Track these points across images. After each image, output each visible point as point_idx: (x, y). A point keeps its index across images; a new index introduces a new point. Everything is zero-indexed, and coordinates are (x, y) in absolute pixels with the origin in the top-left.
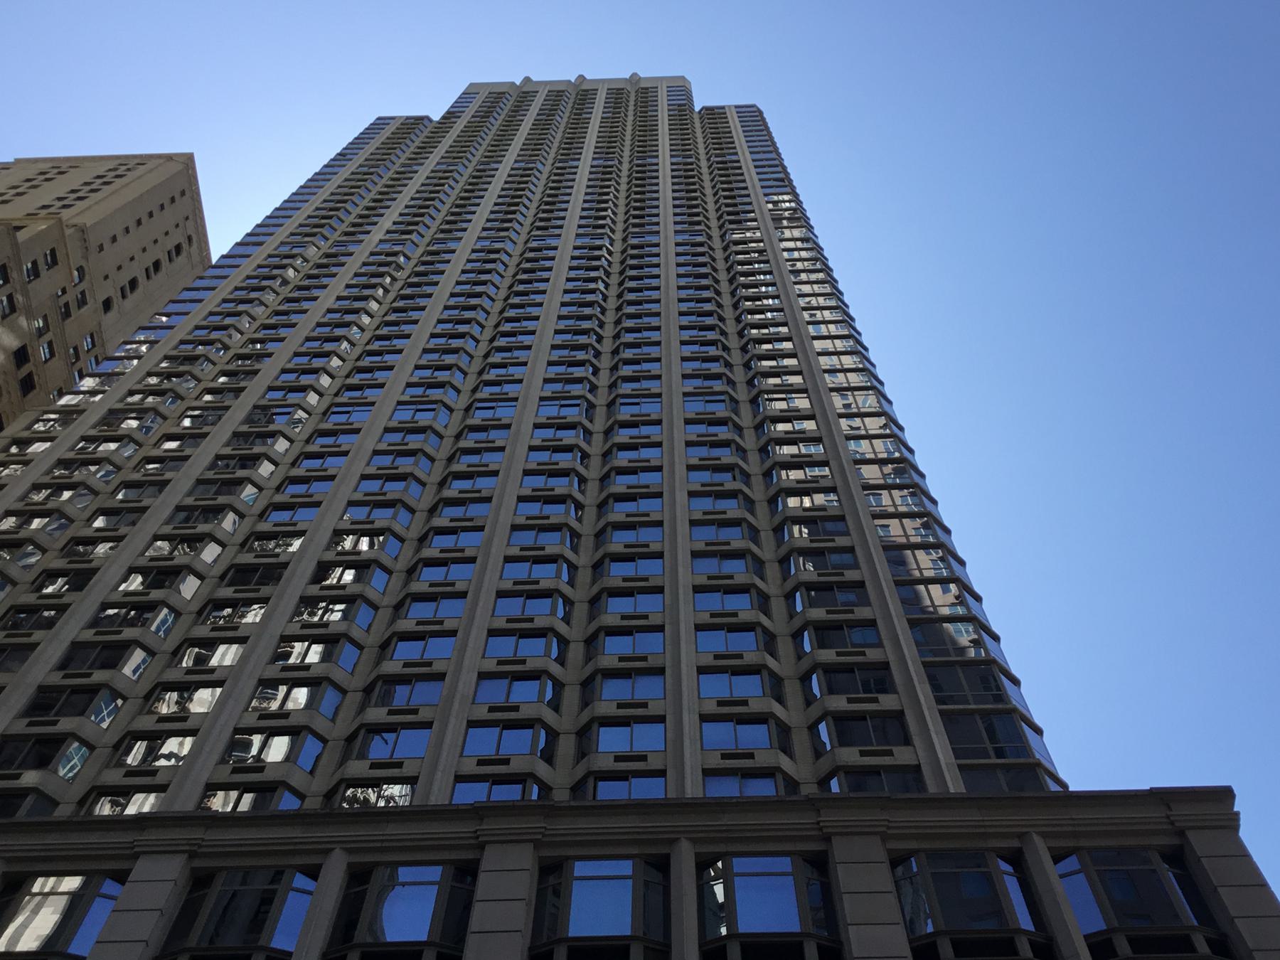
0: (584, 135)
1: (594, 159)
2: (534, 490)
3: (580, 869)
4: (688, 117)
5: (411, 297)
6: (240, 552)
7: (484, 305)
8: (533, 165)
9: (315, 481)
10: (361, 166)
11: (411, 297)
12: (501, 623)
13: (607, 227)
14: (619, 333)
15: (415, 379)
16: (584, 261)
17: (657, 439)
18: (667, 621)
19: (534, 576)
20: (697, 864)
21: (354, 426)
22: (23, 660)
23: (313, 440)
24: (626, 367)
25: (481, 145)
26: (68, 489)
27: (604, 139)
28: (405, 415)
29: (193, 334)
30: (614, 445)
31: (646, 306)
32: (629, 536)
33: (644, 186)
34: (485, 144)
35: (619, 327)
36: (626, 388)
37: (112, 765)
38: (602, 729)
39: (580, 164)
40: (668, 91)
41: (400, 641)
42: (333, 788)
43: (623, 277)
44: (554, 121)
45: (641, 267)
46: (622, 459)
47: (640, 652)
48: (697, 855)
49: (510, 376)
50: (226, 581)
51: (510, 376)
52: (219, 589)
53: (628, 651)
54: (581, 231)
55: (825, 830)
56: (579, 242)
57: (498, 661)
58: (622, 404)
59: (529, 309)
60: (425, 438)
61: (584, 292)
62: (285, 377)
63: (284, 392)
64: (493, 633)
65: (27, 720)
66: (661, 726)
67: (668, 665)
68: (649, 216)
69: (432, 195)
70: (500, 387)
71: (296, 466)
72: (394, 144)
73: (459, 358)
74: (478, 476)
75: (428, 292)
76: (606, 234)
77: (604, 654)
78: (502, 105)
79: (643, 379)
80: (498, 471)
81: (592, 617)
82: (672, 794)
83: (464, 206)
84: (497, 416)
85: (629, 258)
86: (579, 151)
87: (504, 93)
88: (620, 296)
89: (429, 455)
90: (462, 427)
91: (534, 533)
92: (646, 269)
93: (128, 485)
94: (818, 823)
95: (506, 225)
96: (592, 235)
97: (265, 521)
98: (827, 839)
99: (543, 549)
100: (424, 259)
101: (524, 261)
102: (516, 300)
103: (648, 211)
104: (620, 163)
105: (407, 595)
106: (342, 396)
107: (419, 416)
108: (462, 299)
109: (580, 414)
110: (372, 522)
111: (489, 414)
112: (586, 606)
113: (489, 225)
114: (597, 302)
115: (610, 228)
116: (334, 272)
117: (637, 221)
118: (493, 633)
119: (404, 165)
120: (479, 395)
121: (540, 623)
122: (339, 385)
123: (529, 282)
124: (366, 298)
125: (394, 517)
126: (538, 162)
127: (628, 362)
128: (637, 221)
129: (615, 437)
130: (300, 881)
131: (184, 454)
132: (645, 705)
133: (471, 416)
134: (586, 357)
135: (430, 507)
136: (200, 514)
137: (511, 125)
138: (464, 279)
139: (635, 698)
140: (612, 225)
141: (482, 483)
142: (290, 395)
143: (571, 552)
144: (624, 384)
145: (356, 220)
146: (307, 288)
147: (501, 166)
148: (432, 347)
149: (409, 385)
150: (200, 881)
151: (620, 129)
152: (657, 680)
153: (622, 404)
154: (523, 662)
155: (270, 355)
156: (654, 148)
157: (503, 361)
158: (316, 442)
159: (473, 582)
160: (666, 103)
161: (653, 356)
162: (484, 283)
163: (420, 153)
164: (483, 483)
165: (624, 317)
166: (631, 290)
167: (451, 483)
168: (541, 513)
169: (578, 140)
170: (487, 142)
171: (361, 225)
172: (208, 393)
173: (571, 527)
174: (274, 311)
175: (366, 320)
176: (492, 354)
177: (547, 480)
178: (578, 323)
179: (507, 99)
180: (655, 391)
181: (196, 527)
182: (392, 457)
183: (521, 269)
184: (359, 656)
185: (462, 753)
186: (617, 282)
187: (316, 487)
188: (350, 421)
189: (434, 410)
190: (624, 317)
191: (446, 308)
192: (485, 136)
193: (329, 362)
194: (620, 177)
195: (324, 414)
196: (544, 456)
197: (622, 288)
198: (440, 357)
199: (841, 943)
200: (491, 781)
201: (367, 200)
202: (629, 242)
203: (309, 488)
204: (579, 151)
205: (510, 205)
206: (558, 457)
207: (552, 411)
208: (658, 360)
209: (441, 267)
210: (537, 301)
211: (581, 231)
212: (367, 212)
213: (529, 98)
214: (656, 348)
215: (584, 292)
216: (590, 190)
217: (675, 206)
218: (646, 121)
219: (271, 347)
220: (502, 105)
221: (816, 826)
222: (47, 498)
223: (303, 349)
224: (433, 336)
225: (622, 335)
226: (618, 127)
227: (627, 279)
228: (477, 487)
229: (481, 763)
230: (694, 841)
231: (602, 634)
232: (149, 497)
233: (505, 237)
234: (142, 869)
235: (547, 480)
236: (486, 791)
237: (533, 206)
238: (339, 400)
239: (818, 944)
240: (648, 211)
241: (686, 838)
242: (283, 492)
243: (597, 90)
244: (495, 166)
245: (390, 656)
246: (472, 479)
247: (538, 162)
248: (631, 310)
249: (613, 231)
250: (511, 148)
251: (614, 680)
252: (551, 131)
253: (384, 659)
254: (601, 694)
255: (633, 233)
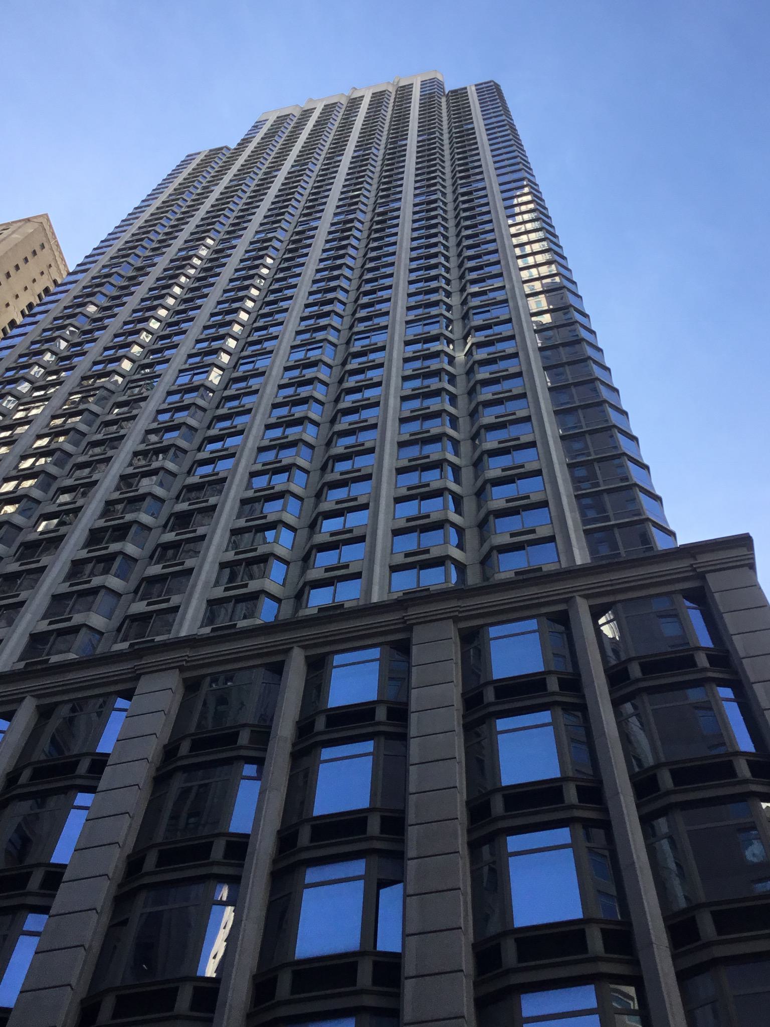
0: (403, 153)
1: (416, 196)
2: (412, 412)
3: (494, 631)
4: (506, 122)
5: (284, 279)
6: (164, 532)
7: (334, 324)
8: (362, 186)
9: (219, 460)
10: (231, 181)
11: (284, 279)
12: (400, 559)
13: (439, 235)
14: (464, 273)
15: (302, 328)
16: (423, 241)
17: (534, 466)
18: (501, 258)
19: (424, 511)
20: (629, 776)
21: (260, 370)
22: (57, 548)
23: (203, 448)
24: (482, 369)
25: (326, 142)
26: (61, 436)
27: (424, 154)
28: (300, 355)
29: (104, 355)
30: (478, 404)
31: (487, 269)
32: (509, 490)
33: (471, 200)
34: (321, 158)
35: (465, 294)
36: (475, 302)
37: (119, 640)
38: (501, 556)
39: (408, 142)
40: (488, 135)
41: (319, 552)
42: (319, 491)
43: (461, 258)
44: (381, 115)
45: (475, 226)
46: (486, 394)
47: (522, 493)
48: (590, 607)
49: (359, 445)
50: (168, 528)
51: (359, 445)
52: (176, 505)
53: (518, 528)
54: (418, 192)
55: (698, 570)
56: (418, 200)
57: (405, 554)
58: (356, 340)
59: (378, 307)
60: (297, 453)
61: (428, 280)
62: (199, 346)
63: (180, 395)
64: (394, 569)
65: (47, 621)
66: (529, 424)
67: (524, 369)
68: (477, 198)
69: (295, 184)
70: (354, 437)
71: (192, 474)
72: (254, 159)
73: (314, 389)
74: (368, 370)
75: (297, 272)
76: (439, 189)
77: (496, 534)
78: (338, 109)
79: (497, 342)
80: (387, 326)
81: (483, 540)
82: (564, 565)
83: (318, 193)
84: (373, 342)
85: (465, 249)
86: (399, 183)
87: (336, 103)
88: (460, 266)
89: (309, 444)
90: (314, 515)
91: (416, 502)
92: (477, 209)
93: (119, 405)
94: (691, 565)
95: (336, 273)
96: (428, 192)
97: (193, 475)
98: (702, 577)
99: (429, 408)
100: (286, 256)
101: (368, 261)
102: (368, 287)
103: (479, 219)
104: (442, 134)
105: (305, 584)
106: (230, 389)
107: (310, 354)
108: (323, 284)
109: (440, 328)
110: (273, 488)
111: (366, 342)
112: (478, 567)
113: (328, 246)
114: (440, 252)
115: (443, 235)
116: (206, 293)
117: (467, 214)
118: (394, 569)
119: (266, 174)
120: (356, 330)
121: (435, 553)
122: (210, 417)
123: (381, 238)
124: (257, 267)
125: (284, 509)
126: (373, 148)
127: (485, 383)
128: (467, 214)
129: (478, 397)
130: (121, 703)
131: (106, 456)
132: (533, 531)
133: (311, 567)
134: (439, 348)
135: (295, 593)
136: (152, 456)
137: (346, 126)
138: (322, 267)
139: (531, 565)
140: (444, 242)
141: (369, 393)
142: (186, 396)
143: (456, 515)
144: (483, 389)
145: (259, 183)
146: (168, 336)
147: (343, 158)
148: (303, 328)
149: (281, 387)
150: (191, 687)
151: (437, 120)
152: (532, 451)
153: (474, 314)
154: (427, 551)
155: (159, 376)
156: (477, 170)
157: (354, 405)
158: (216, 427)
159: (378, 440)
160: (485, 138)
161: (515, 392)
162: (327, 314)
163: (290, 139)
164: (361, 462)
165: (469, 297)
166: (472, 270)
167: (336, 443)
168: (421, 454)
169: (399, 160)
170: (323, 156)
171: (247, 210)
172: (63, 493)
173: (455, 559)
174: (166, 324)
175: (265, 271)
176: (346, 379)
177: (420, 505)
178: (426, 346)
179: (333, 119)
180: (510, 351)
181: (71, 618)
182: (267, 476)
183: (366, 269)
184: (307, 480)
185: (394, 517)
186: (453, 216)
187: (230, 442)
188: (256, 367)
189: (321, 347)
190: (469, 297)
191: (303, 319)
192: (321, 147)
193: (232, 329)
194: (443, 162)
195: (235, 367)
196: (416, 404)
197: (463, 269)
198: (312, 335)
199: (728, 651)
200: (418, 567)
201: (256, 181)
202: (460, 192)
203: (215, 467)
204: (399, 183)
205: (343, 231)
206: (428, 402)
207: (418, 329)
208: (512, 337)
209: (293, 281)
210: (391, 251)
211: (418, 192)
212: (250, 200)
213: (352, 115)
214: (517, 381)
215: (428, 280)
216: (418, 185)
217: (491, 145)
218: (459, 102)
219: (159, 368)
220: (338, 109)
221: (690, 569)
222: (50, 442)
223: (203, 336)
224: (311, 293)
225: (474, 353)
226: (434, 111)
227: (464, 239)
228: (353, 494)
229: (407, 555)
230: (587, 597)
231: (488, 486)
232: (27, 589)
233: (355, 209)
234: (143, 685)
235: (420, 505)
236: (416, 540)
237: (375, 183)
238: (245, 353)
239: (706, 654)
240: (479, 219)
241: (579, 596)
242: (204, 451)
243: (412, 84)
244: (339, 158)
245: (318, 530)
246: (358, 412)
247: (358, 211)
248: (474, 275)
249: (446, 238)
250: (347, 147)
251: (493, 432)
252: (369, 167)
253: (314, 534)
254: (499, 567)
255: (461, 184)
